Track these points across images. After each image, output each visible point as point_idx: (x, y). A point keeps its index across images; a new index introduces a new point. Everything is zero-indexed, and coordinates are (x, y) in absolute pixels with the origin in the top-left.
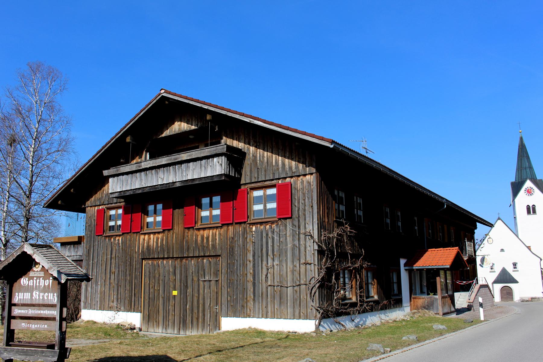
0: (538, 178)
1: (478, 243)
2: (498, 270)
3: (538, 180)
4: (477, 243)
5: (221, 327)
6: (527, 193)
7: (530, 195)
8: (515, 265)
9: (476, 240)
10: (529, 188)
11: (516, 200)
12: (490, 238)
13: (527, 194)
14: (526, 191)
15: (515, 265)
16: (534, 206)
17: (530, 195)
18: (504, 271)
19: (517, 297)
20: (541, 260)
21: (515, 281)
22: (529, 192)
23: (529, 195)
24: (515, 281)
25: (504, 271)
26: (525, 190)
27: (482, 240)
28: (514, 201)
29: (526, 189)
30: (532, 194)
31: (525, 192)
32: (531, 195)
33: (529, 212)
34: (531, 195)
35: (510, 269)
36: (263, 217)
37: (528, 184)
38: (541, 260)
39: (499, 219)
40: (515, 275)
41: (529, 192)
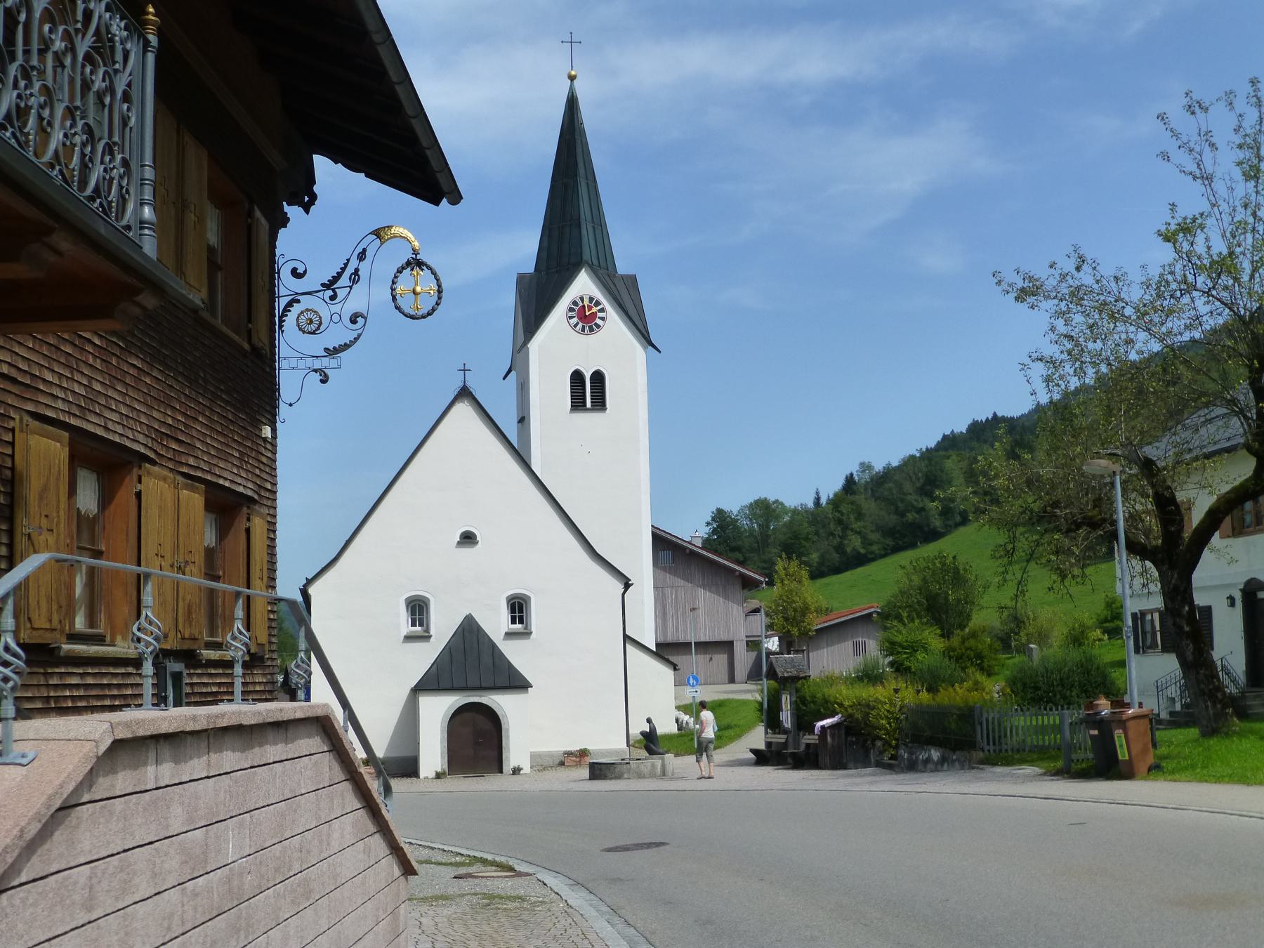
0: (622, 267)
1: (306, 302)
2: (443, 626)
3: (622, 276)
4: (296, 309)
5: (436, 696)
6: (575, 320)
7: (587, 329)
8: (518, 608)
9: (285, 273)
10: (586, 302)
11: (534, 345)
12: (420, 264)
13: (576, 326)
14: (574, 314)
15: (518, 608)
16: (598, 378)
17: (587, 329)
18: (469, 632)
19: (517, 751)
20: (627, 585)
21: (517, 683)
22: (586, 318)
23: (583, 329)
24: (517, 683)
25: (469, 632)
26: (571, 310)
27: (344, 280)
28: (525, 348)
29: (575, 303)
30: (596, 324)
31: (571, 314)
32: (591, 329)
33: (578, 404)
34: (591, 329)
35: (496, 624)
36: (218, 639)
37: (583, 285)
38: (627, 585)
39: (465, 393)
40: (517, 654)
41: (586, 318)
